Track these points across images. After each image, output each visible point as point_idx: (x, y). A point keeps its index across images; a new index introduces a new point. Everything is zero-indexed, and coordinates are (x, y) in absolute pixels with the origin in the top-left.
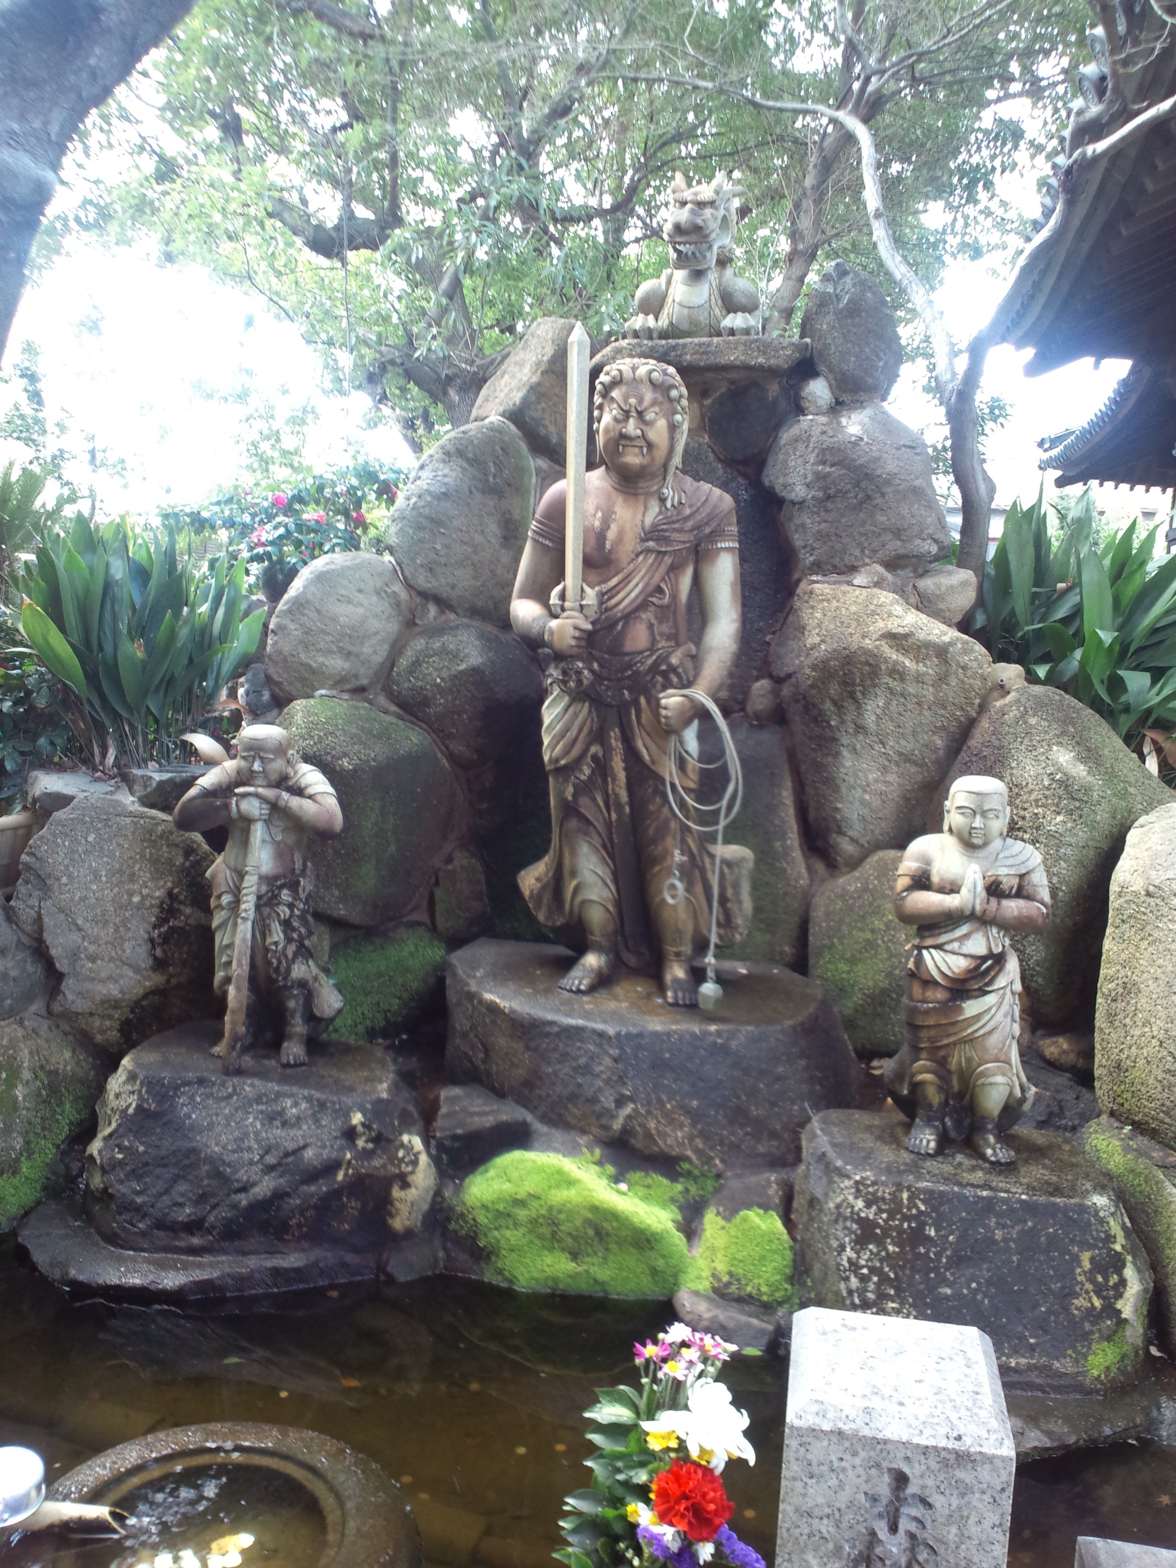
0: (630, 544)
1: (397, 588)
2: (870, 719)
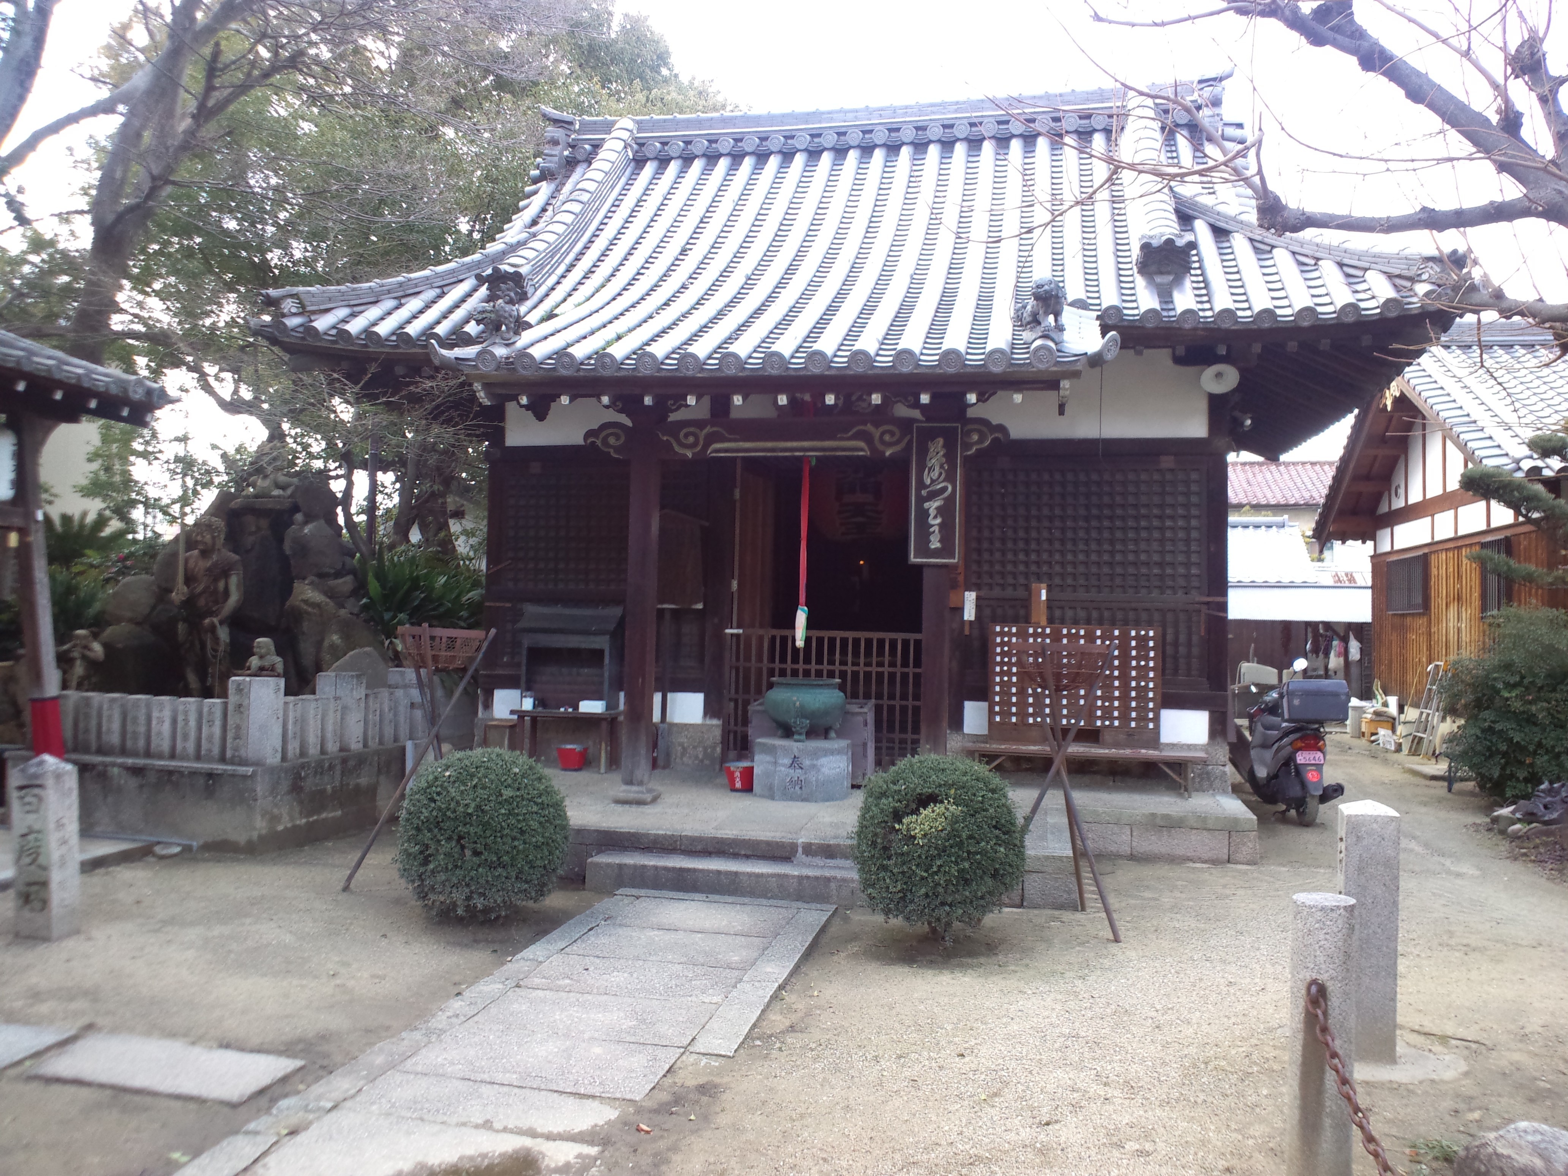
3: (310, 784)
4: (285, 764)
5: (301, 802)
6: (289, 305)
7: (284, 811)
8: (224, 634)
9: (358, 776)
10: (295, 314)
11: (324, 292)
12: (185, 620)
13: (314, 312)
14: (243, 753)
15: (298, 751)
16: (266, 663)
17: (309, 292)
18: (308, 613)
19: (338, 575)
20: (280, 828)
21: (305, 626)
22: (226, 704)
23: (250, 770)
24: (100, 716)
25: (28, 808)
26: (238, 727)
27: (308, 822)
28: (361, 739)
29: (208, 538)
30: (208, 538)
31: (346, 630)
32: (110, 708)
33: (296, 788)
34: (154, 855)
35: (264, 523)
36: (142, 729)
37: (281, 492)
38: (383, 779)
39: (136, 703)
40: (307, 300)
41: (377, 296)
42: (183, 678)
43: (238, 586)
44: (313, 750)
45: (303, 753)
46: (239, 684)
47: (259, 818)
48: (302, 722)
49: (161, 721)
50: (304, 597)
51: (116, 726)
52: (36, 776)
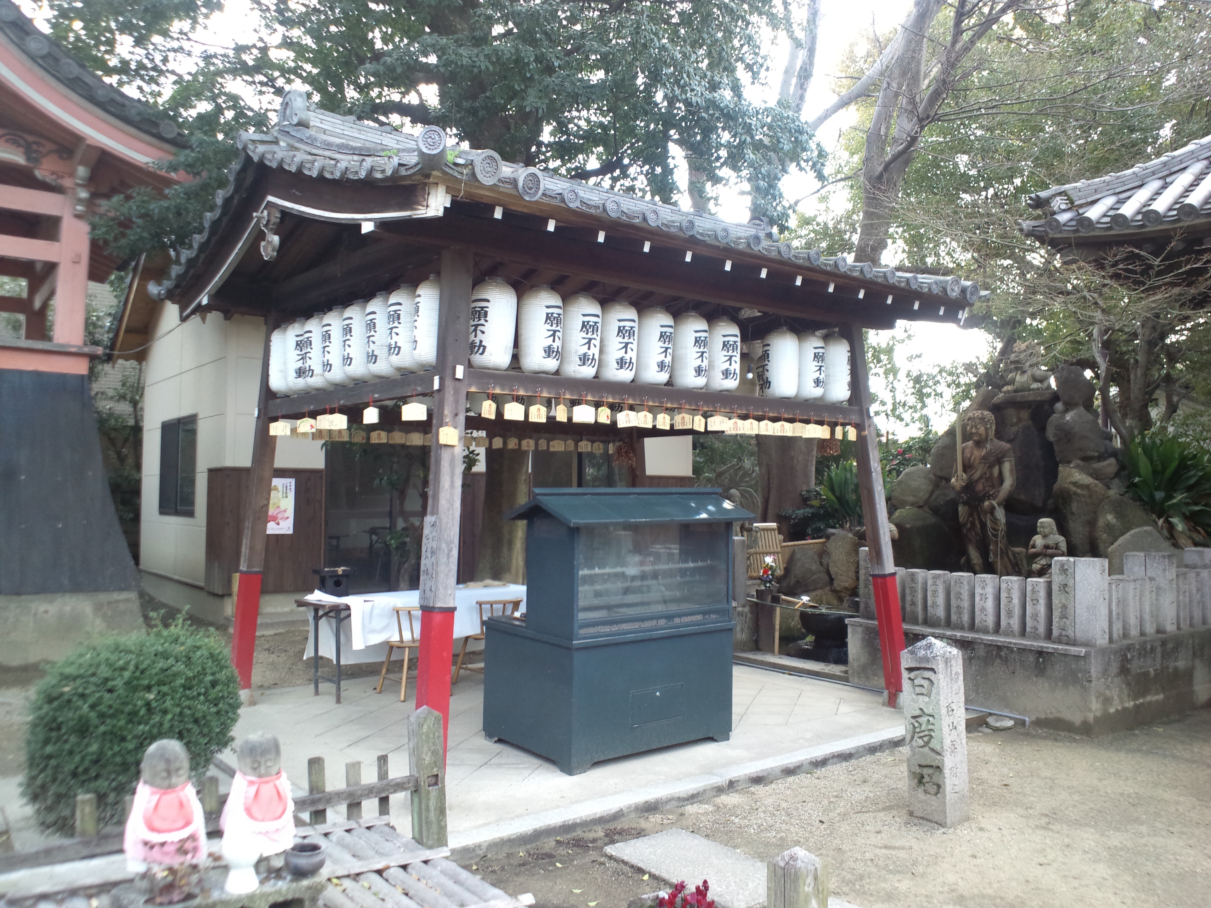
0: (977, 461)
1: (931, 476)
2: (1074, 510)
3: (1135, 666)
4: (1113, 646)
5: (1128, 684)
6: (1058, 203)
7: (1114, 693)
8: (1000, 514)
9: (1176, 660)
10: (1064, 211)
11: (1089, 185)
12: (965, 503)
13: (1081, 206)
14: (1070, 633)
15: (1121, 632)
16: (1051, 541)
17: (1075, 188)
18: (1075, 494)
19: (1101, 458)
20: (1112, 710)
21: (1074, 506)
22: (1049, 585)
23: (1082, 651)
24: (925, 591)
25: (918, 690)
26: (1064, 607)
27: (1135, 704)
28: (1175, 621)
29: (982, 430)
30: (982, 430)
31: (1119, 510)
32: (935, 584)
33: (1124, 671)
34: (988, 725)
35: (1025, 414)
36: (966, 604)
37: (1039, 385)
38: (1198, 663)
39: (959, 581)
40: (1074, 196)
41: (1142, 180)
42: (964, 552)
43: (1011, 471)
44: (1134, 632)
45: (1125, 635)
46: (1062, 565)
47: (1094, 700)
48: (1122, 602)
49: (984, 597)
50: (1072, 480)
51: (941, 600)
52: (926, 659)
